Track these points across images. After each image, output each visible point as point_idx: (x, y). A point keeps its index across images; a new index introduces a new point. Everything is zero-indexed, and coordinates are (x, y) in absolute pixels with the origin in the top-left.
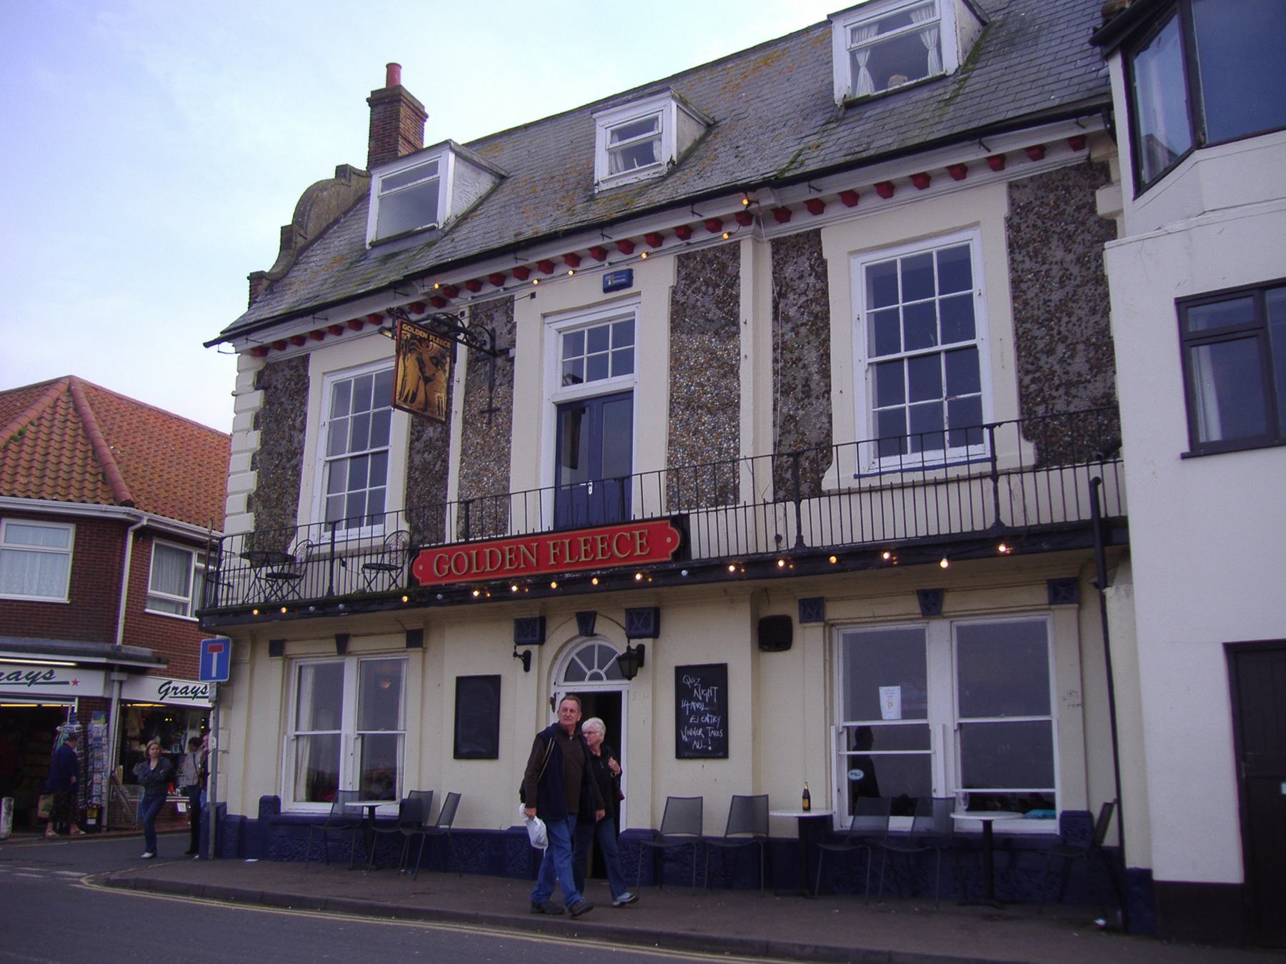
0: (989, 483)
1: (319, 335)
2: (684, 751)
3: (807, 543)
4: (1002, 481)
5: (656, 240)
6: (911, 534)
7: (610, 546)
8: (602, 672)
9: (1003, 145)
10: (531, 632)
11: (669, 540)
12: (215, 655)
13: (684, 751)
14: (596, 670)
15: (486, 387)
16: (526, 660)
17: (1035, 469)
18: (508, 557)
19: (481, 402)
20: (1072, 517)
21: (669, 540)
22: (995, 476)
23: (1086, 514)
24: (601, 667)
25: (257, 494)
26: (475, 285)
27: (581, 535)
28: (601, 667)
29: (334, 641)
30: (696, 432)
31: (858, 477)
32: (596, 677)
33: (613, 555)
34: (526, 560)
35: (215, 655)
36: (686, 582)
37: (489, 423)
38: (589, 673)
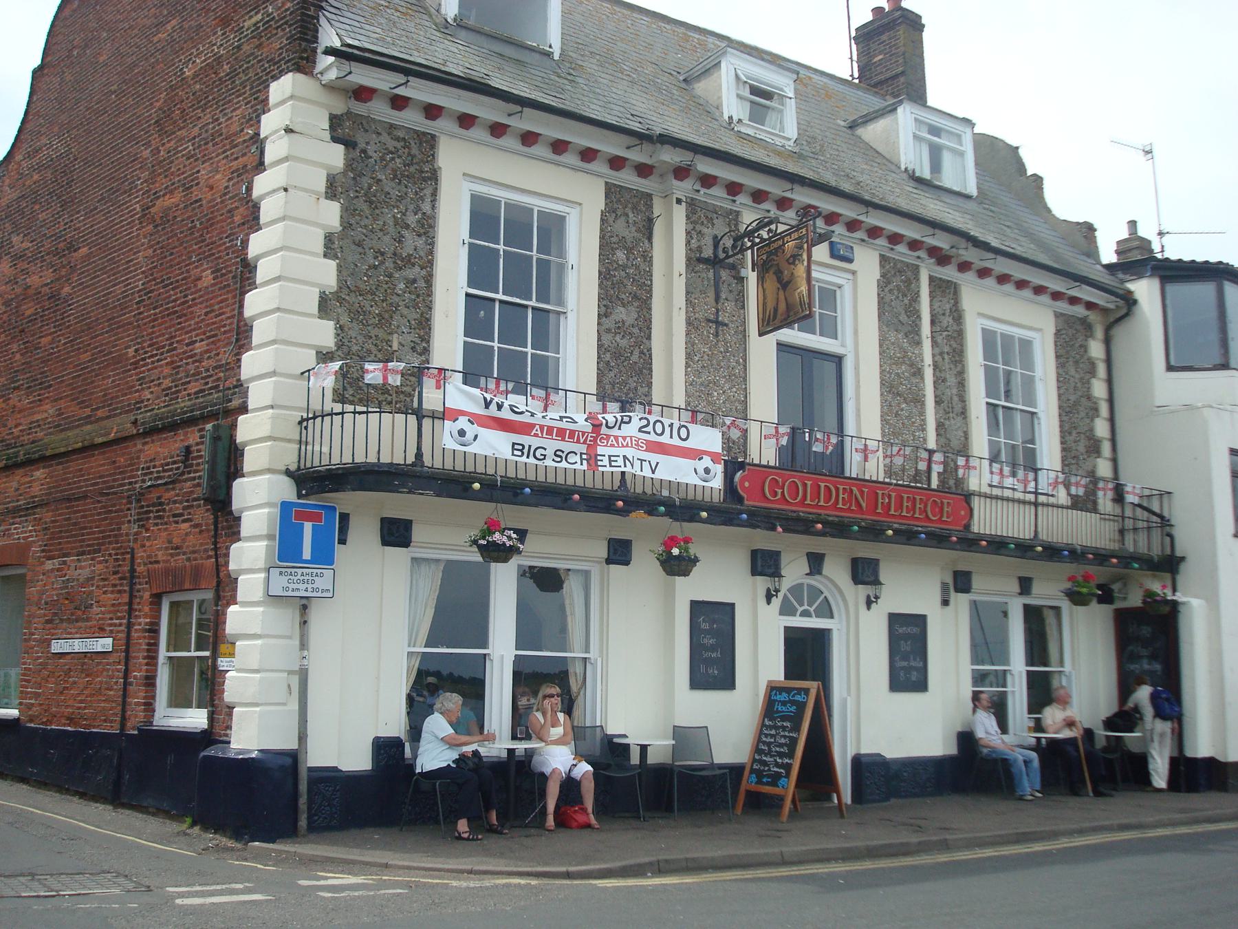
0: (1033, 508)
1: (466, 121)
2: (698, 682)
3: (427, 460)
4: (1040, 508)
5: (874, 232)
6: (360, 459)
7: (925, 507)
8: (812, 610)
9: (705, 166)
10: (764, 564)
11: (747, 484)
12: (308, 527)
13: (698, 682)
14: (806, 607)
15: (712, 294)
16: (945, 603)
17: (1067, 508)
18: (841, 496)
19: (706, 308)
20: (398, 459)
21: (747, 484)
22: (1036, 504)
23: (411, 459)
24: (810, 605)
25: (337, 295)
26: (708, 181)
27: (823, 481)
28: (810, 605)
29: (605, 543)
30: (897, 415)
31: (990, 486)
32: (806, 614)
33: (927, 516)
34: (859, 505)
35: (308, 527)
36: (889, 540)
37: (717, 335)
38: (800, 609)
